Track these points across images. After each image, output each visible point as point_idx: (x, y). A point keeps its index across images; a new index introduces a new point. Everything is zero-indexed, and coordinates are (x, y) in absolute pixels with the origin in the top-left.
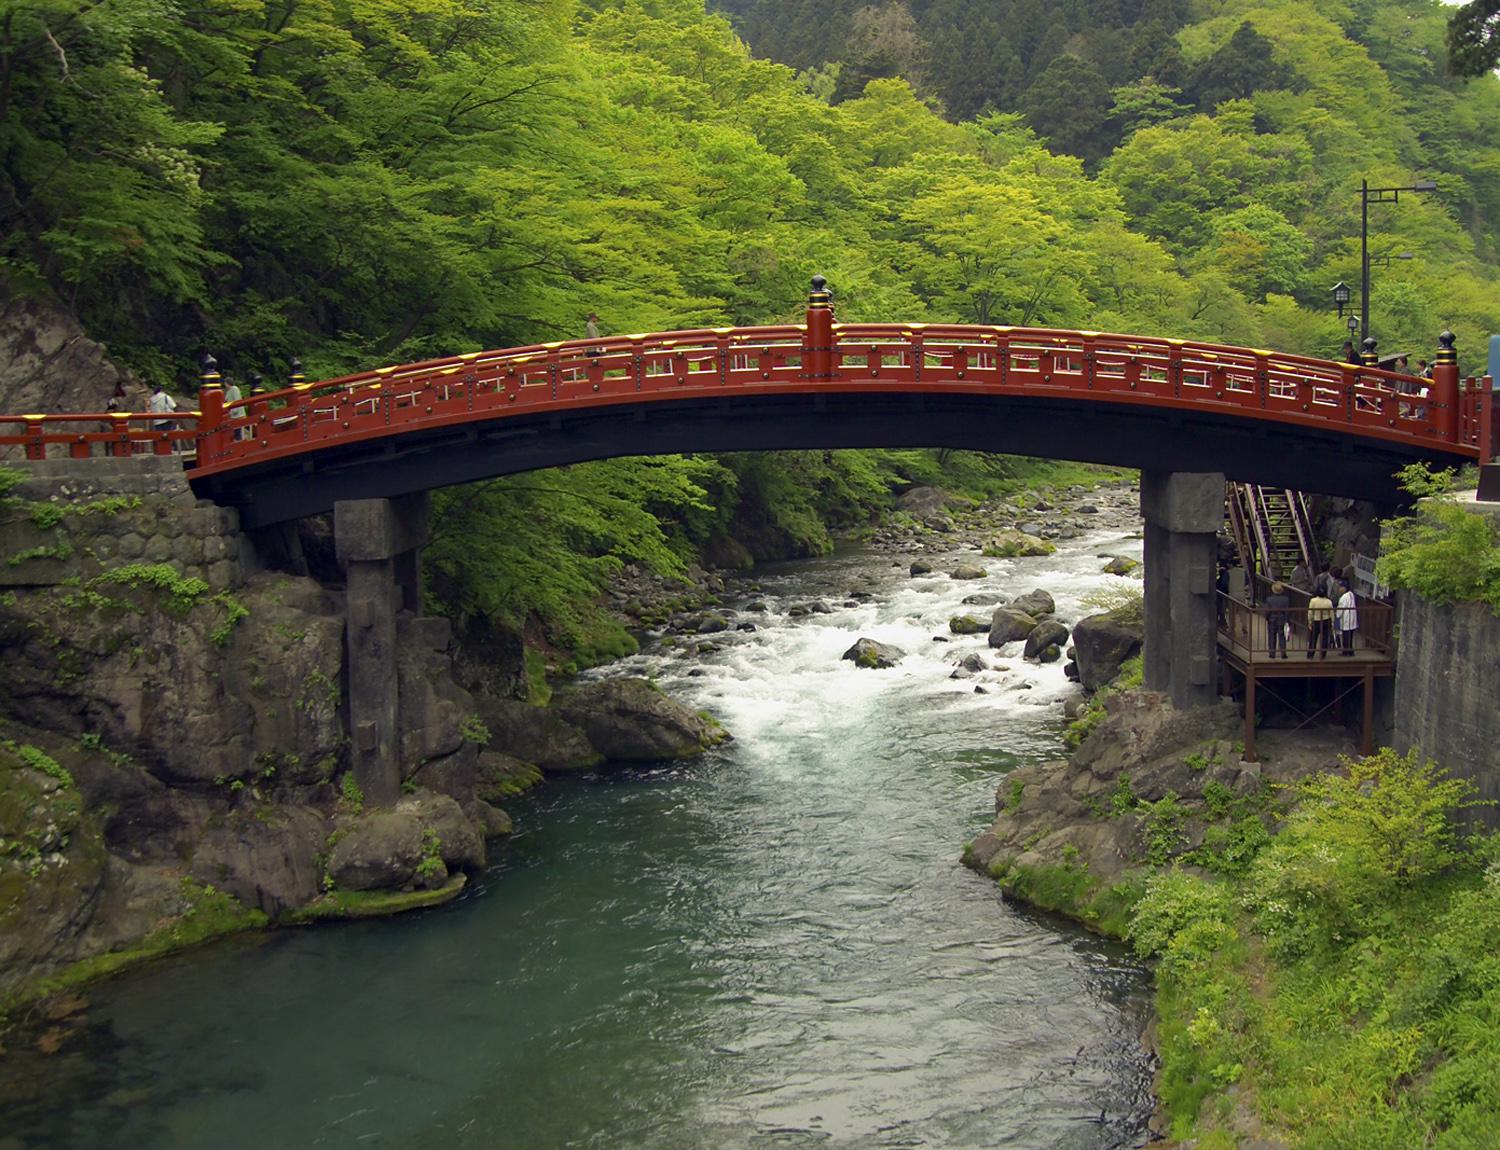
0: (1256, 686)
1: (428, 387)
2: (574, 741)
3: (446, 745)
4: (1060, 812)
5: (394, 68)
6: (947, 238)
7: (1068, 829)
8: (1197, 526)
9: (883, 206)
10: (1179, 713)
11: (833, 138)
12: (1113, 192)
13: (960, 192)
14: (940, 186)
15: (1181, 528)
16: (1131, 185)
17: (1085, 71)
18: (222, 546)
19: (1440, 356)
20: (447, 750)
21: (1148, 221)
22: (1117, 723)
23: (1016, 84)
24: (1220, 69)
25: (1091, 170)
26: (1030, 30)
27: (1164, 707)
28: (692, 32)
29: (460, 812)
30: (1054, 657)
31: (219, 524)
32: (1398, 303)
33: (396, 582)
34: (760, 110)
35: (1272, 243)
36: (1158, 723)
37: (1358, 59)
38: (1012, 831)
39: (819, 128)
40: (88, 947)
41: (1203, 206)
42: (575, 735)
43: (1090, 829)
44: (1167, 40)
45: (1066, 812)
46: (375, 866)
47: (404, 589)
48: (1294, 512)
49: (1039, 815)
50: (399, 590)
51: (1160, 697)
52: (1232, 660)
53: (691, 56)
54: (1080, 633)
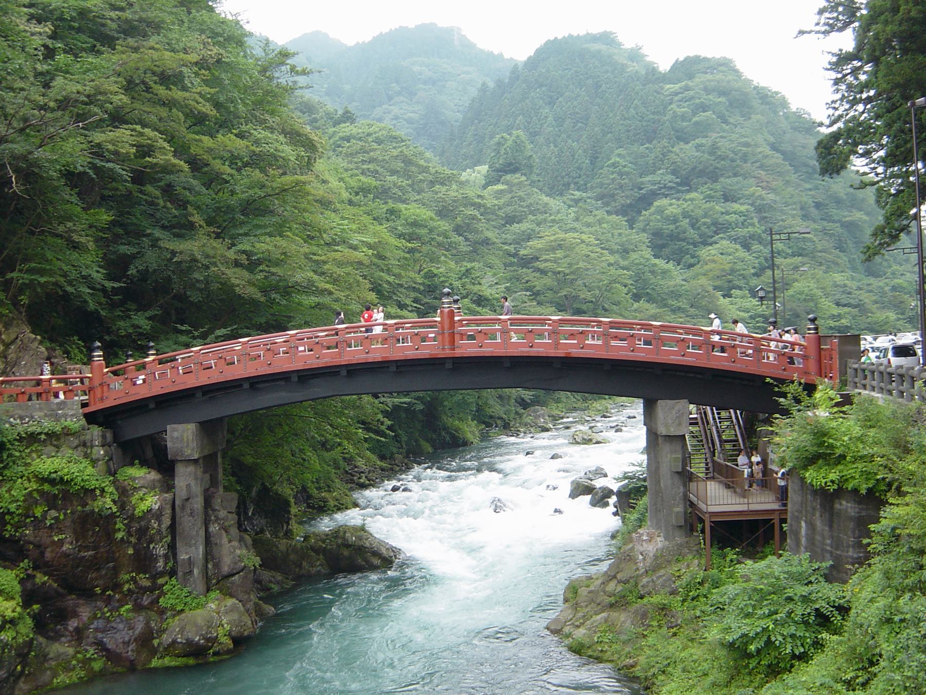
0: (711, 526)
1: (269, 350)
2: (318, 563)
3: (233, 569)
4: (599, 604)
5: (213, 180)
6: (547, 264)
7: (603, 615)
8: (673, 431)
9: (511, 249)
10: (667, 543)
11: (482, 210)
12: (644, 237)
13: (552, 238)
14: (542, 234)
15: (664, 433)
16: (653, 234)
17: (626, 169)
18: (102, 452)
19: (809, 329)
20: (235, 571)
21: (667, 251)
22: (632, 549)
23: (588, 176)
24: (701, 167)
25: (631, 224)
26: (594, 147)
27: (659, 539)
28: (401, 152)
29: (242, 609)
30: (606, 505)
31: (100, 439)
32: (807, 295)
33: (205, 472)
34: (440, 195)
35: (735, 263)
36: (655, 549)
37: (777, 161)
38: (571, 616)
39: (473, 204)
40: (21, 689)
41: (695, 244)
42: (318, 560)
43: (616, 614)
44: (671, 152)
45: (603, 604)
46: (189, 642)
47: (211, 475)
48: (734, 420)
49: (587, 606)
50: (207, 476)
51: (656, 533)
52: (699, 511)
53: (399, 165)
54: (619, 494)
